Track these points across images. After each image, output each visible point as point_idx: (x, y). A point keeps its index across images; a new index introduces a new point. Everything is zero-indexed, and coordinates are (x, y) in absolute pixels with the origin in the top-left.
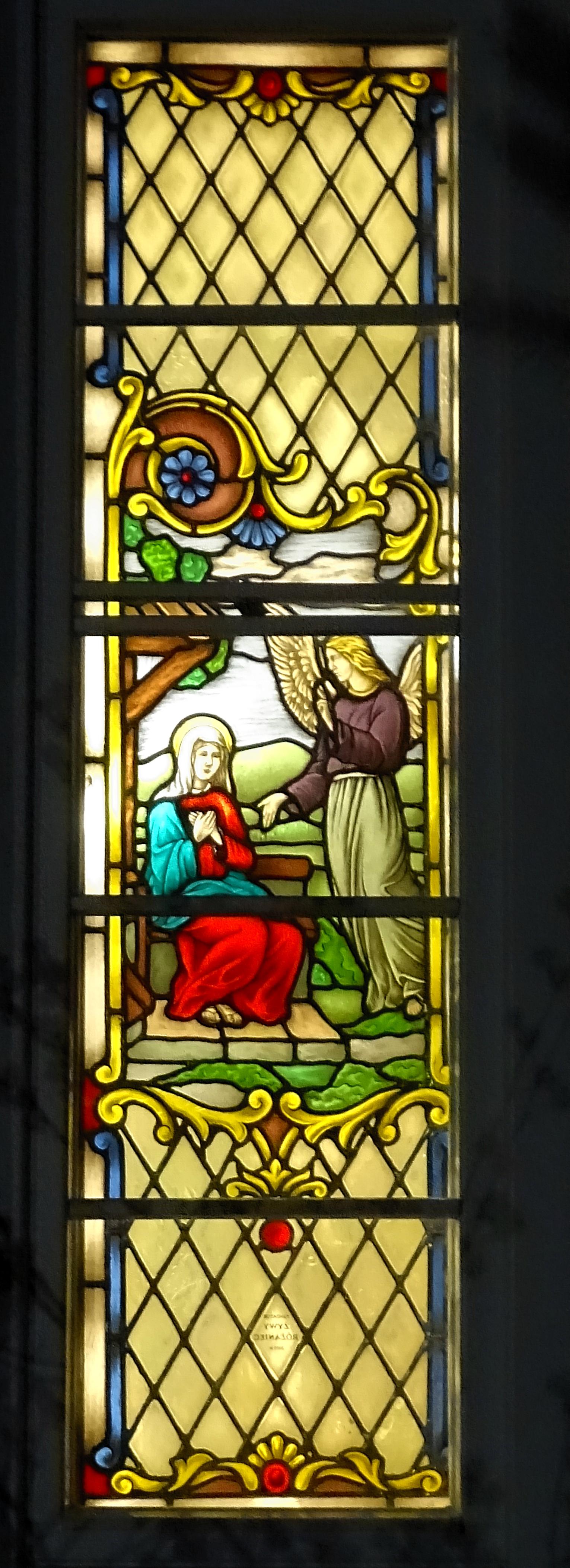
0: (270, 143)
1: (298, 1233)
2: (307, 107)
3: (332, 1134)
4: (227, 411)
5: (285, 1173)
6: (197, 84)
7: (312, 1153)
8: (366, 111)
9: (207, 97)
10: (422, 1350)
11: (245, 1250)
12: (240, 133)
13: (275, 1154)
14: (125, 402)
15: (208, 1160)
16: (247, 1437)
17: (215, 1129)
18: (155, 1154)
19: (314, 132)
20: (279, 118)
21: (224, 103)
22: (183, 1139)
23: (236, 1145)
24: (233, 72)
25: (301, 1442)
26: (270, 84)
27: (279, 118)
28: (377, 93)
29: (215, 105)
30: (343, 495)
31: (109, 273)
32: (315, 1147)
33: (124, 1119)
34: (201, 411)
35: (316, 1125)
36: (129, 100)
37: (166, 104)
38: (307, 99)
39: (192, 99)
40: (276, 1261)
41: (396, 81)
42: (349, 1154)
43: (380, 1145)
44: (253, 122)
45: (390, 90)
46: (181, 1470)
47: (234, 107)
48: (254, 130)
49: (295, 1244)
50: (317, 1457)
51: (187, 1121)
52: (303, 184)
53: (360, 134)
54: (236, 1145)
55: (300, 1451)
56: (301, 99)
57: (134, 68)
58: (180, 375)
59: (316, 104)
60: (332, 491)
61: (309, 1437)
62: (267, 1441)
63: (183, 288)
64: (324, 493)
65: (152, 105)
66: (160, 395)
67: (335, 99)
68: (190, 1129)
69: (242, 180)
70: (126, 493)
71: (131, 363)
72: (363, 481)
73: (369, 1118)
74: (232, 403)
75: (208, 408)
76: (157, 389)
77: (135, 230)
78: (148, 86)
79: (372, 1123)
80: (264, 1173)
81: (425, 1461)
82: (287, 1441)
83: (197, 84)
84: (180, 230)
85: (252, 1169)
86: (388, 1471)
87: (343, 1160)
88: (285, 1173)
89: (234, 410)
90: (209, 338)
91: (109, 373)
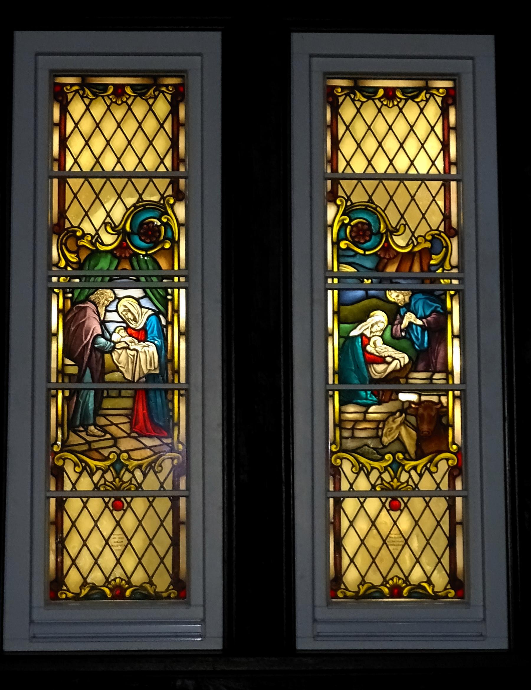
0: (390, 114)
1: (403, 505)
2: (403, 102)
3: (415, 468)
4: (375, 209)
5: (399, 483)
6: (365, 93)
7: (131, 475)
8: (424, 103)
9: (96, 95)
10: (447, 546)
11: (384, 510)
12: (109, 109)
13: (395, 477)
14: (338, 207)
15: (371, 479)
16: (107, 579)
17: (373, 468)
18: (351, 476)
19: (134, 108)
20: (123, 102)
21: (103, 97)
22: (362, 472)
23: (381, 473)
24: (377, 89)
25: (404, 579)
26: (390, 94)
27: (394, 105)
28: (428, 96)
29: (370, 102)
30: (416, 239)
31: (333, 162)
32: (132, 473)
33: (64, 464)
34: (366, 209)
35: (409, 464)
36: (341, 99)
37: (353, 100)
38: (133, 96)
39: (91, 96)
40: (118, 514)
41: (434, 92)
42: (421, 476)
43: (431, 473)
44: (113, 104)
45: (432, 95)
46: (83, 591)
47: (106, 98)
48: (113, 107)
49: (402, 508)
50: (410, 585)
51: (363, 465)
52: (401, 128)
53: (422, 110)
54: (381, 473)
55: (404, 582)
56: (401, 99)
57: (72, 85)
58: (359, 197)
59: (135, 97)
60: (413, 238)
61: (129, 578)
62: (392, 579)
63: (86, 162)
64: (411, 239)
65: (77, 98)
66: (352, 203)
67: (413, 98)
68: (364, 468)
69: (380, 127)
70: (339, 240)
71: (341, 193)
72: (86, 232)
73: (427, 463)
74: (377, 206)
75: (369, 208)
76: (351, 201)
77: (342, 146)
78: (77, 91)
79: (153, 465)
80: (391, 483)
81: (449, 587)
82: (122, 580)
83: (365, 93)
84: (108, 142)
85: (388, 481)
86: (435, 590)
87: (418, 478)
88: (399, 483)
89: (378, 209)
90: (370, 185)
91: (333, 197)
